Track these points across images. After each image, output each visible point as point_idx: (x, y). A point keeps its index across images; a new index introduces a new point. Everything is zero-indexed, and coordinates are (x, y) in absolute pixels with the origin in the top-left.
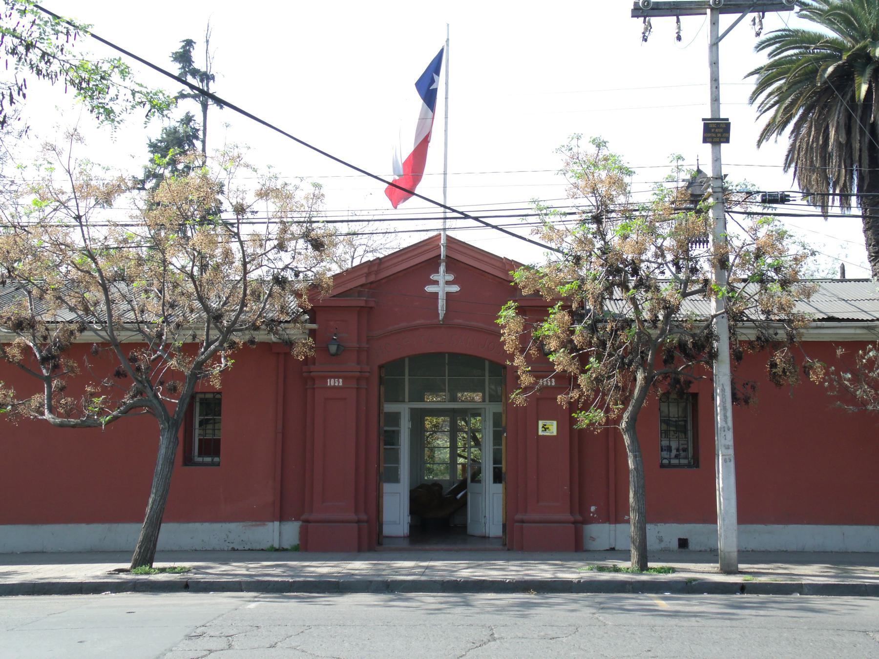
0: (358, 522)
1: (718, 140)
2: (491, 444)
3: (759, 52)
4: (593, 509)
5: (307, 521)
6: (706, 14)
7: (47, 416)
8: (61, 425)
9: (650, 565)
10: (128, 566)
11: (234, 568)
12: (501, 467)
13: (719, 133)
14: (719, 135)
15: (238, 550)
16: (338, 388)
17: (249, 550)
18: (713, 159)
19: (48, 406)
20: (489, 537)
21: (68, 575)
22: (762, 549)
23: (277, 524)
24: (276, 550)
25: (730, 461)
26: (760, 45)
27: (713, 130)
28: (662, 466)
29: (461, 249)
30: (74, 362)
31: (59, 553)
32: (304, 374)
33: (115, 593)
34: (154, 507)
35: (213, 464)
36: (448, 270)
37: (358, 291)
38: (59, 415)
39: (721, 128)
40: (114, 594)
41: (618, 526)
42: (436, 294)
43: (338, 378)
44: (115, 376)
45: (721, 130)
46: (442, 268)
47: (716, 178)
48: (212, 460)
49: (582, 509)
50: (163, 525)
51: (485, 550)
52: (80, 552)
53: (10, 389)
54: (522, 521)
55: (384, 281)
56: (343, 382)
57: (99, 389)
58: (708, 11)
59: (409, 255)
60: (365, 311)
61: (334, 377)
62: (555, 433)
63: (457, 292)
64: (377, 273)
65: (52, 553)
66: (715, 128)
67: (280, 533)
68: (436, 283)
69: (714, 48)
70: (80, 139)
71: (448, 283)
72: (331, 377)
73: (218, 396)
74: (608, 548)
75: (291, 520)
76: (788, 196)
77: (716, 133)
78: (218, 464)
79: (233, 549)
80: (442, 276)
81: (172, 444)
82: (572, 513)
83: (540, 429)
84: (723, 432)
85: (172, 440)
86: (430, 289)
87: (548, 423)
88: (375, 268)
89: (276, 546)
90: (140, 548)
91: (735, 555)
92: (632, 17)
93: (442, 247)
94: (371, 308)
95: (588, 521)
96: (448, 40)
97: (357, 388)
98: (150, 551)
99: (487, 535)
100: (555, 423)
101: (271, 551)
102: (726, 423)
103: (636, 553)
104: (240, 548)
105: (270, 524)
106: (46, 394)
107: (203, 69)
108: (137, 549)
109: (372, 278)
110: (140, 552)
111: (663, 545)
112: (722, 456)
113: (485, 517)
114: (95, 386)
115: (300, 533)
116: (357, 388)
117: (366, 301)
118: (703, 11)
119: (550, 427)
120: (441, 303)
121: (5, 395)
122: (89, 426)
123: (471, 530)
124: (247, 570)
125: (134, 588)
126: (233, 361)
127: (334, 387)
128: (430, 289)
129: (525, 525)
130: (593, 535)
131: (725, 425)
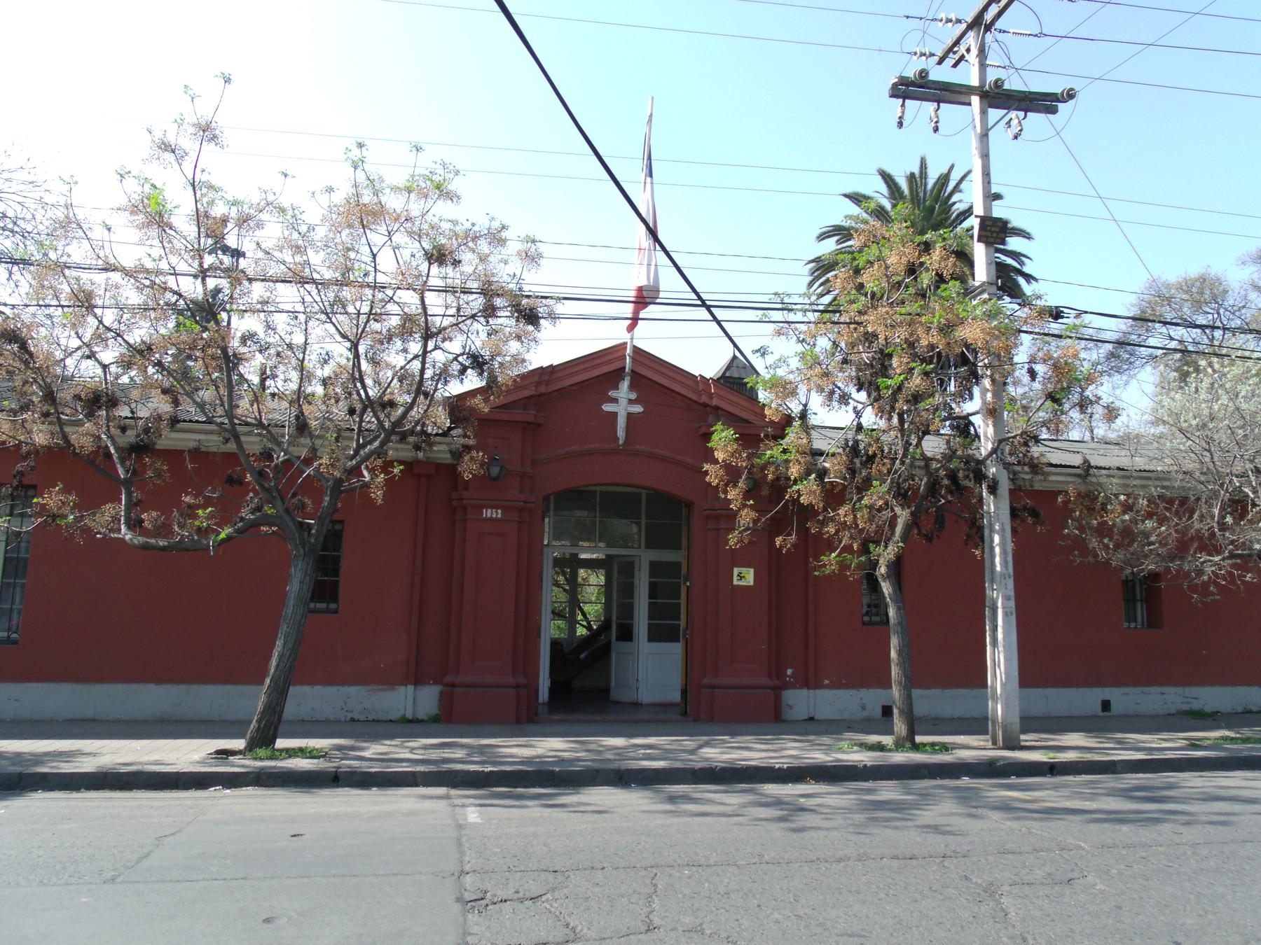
0: (517, 686)
1: (993, 240)
2: (647, 597)
3: (822, 242)
4: (789, 672)
5: (453, 685)
6: (969, 104)
7: (125, 534)
8: (146, 547)
9: (918, 739)
10: (239, 744)
11: (392, 749)
12: (679, 625)
13: (995, 232)
14: (995, 235)
15: (358, 720)
16: (496, 520)
17: (373, 720)
18: (987, 261)
19: (125, 520)
20: (641, 704)
21: (166, 759)
22: (969, 716)
23: (411, 688)
24: (410, 721)
25: (1012, 614)
26: (821, 235)
27: (989, 228)
28: (864, 623)
29: (647, 362)
30: (163, 464)
31: (51, 722)
32: (455, 502)
33: (229, 788)
34: (282, 664)
35: (328, 611)
36: (632, 387)
37: (526, 403)
38: (145, 532)
39: (998, 227)
40: (228, 791)
41: (818, 691)
42: (616, 414)
43: (497, 507)
44: (226, 482)
45: (997, 230)
46: (625, 385)
47: (991, 284)
48: (328, 606)
49: (780, 674)
50: (291, 688)
51: (637, 722)
52: (146, 721)
53: (70, 494)
54: (713, 687)
55: (555, 394)
56: (502, 513)
57: (201, 500)
58: (975, 100)
59: (586, 366)
60: (532, 429)
61: (492, 507)
62: (752, 583)
63: (639, 413)
64: (547, 383)
65: (107, 721)
66: (992, 226)
67: (414, 699)
68: (615, 401)
69: (985, 138)
70: (214, 138)
71: (631, 402)
72: (487, 507)
73: (338, 527)
74: (806, 717)
75: (428, 684)
76: (1062, 312)
77: (992, 232)
78: (336, 612)
79: (353, 720)
80: (624, 391)
81: (308, 578)
82: (770, 677)
83: (735, 578)
84: (1003, 580)
85: (309, 572)
86: (607, 407)
87: (744, 570)
88: (546, 378)
89: (409, 715)
90: (259, 721)
91: (1017, 726)
92: (891, 96)
93: (628, 357)
94: (540, 425)
95: (787, 686)
96: (651, 115)
97: (519, 522)
98: (273, 727)
99: (640, 702)
100: (752, 571)
101: (403, 722)
102: (1007, 569)
103: (903, 727)
104: (363, 718)
105: (402, 689)
106: (123, 503)
107: (234, 246)
108: (254, 725)
109: (543, 389)
110: (259, 727)
111: (866, 714)
112: (1003, 608)
113: (637, 680)
114: (196, 497)
115: (440, 700)
116: (519, 522)
117: (535, 416)
118: (963, 98)
119: (746, 576)
120: (621, 423)
121: (63, 503)
122: (187, 550)
123: (617, 694)
124: (411, 752)
125: (258, 781)
126: (402, 467)
127: (491, 519)
128: (607, 407)
129: (717, 690)
130: (791, 703)
131: (1006, 572)
